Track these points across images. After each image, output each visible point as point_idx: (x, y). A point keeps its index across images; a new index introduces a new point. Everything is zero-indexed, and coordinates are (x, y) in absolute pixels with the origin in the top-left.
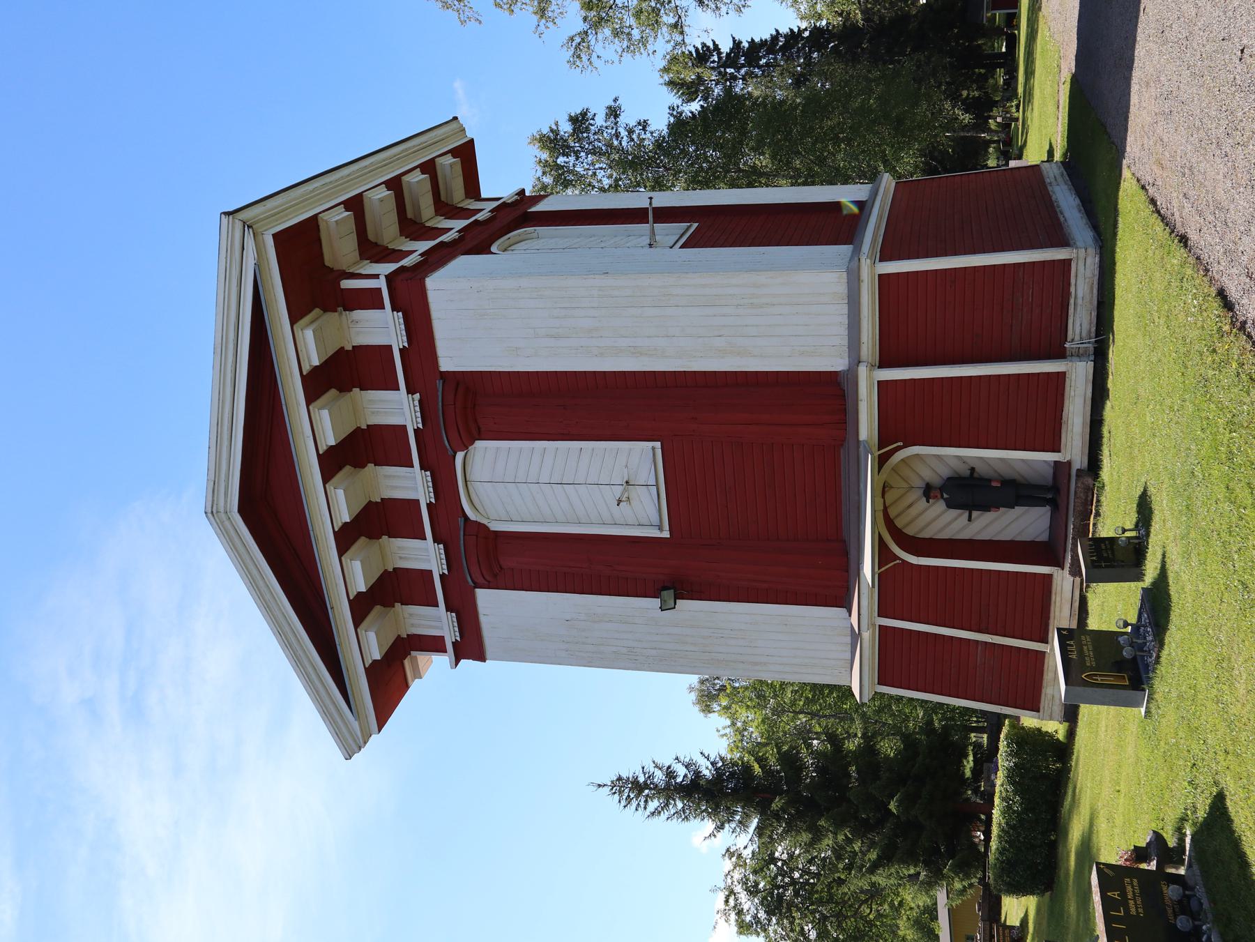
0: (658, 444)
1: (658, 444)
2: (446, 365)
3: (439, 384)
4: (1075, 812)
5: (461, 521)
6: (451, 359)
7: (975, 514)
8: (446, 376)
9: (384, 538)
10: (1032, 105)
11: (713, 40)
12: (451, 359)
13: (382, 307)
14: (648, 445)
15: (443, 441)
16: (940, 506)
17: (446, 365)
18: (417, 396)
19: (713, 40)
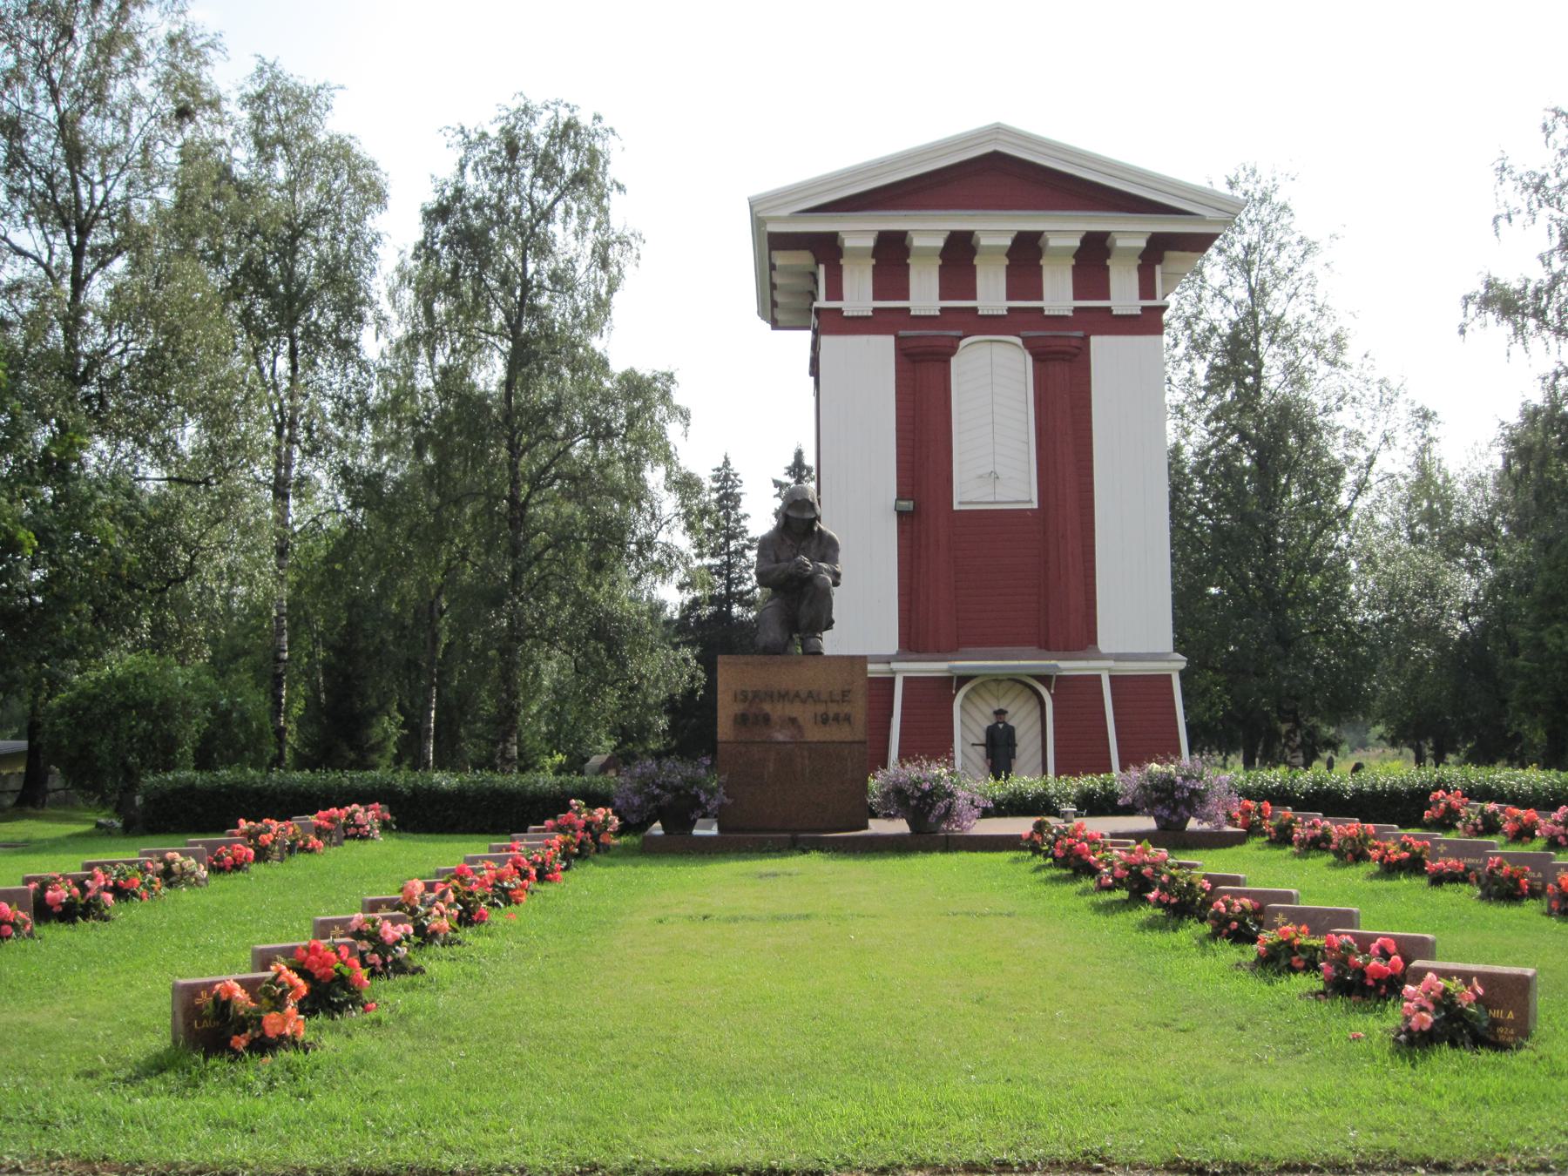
0: (1035, 506)
1: (1035, 506)
2: (1095, 341)
3: (1079, 334)
4: (531, 788)
5: (959, 333)
6: (1102, 347)
7: (982, 750)
8: (1085, 340)
9: (873, 262)
10: (1022, 675)
11: (726, 458)
12: (1102, 347)
13: (1076, 298)
14: (1035, 498)
15: (1038, 329)
16: (986, 723)
17: (1095, 341)
18: (1071, 314)
19: (726, 458)
